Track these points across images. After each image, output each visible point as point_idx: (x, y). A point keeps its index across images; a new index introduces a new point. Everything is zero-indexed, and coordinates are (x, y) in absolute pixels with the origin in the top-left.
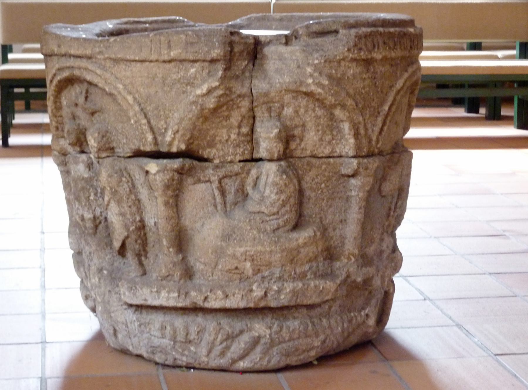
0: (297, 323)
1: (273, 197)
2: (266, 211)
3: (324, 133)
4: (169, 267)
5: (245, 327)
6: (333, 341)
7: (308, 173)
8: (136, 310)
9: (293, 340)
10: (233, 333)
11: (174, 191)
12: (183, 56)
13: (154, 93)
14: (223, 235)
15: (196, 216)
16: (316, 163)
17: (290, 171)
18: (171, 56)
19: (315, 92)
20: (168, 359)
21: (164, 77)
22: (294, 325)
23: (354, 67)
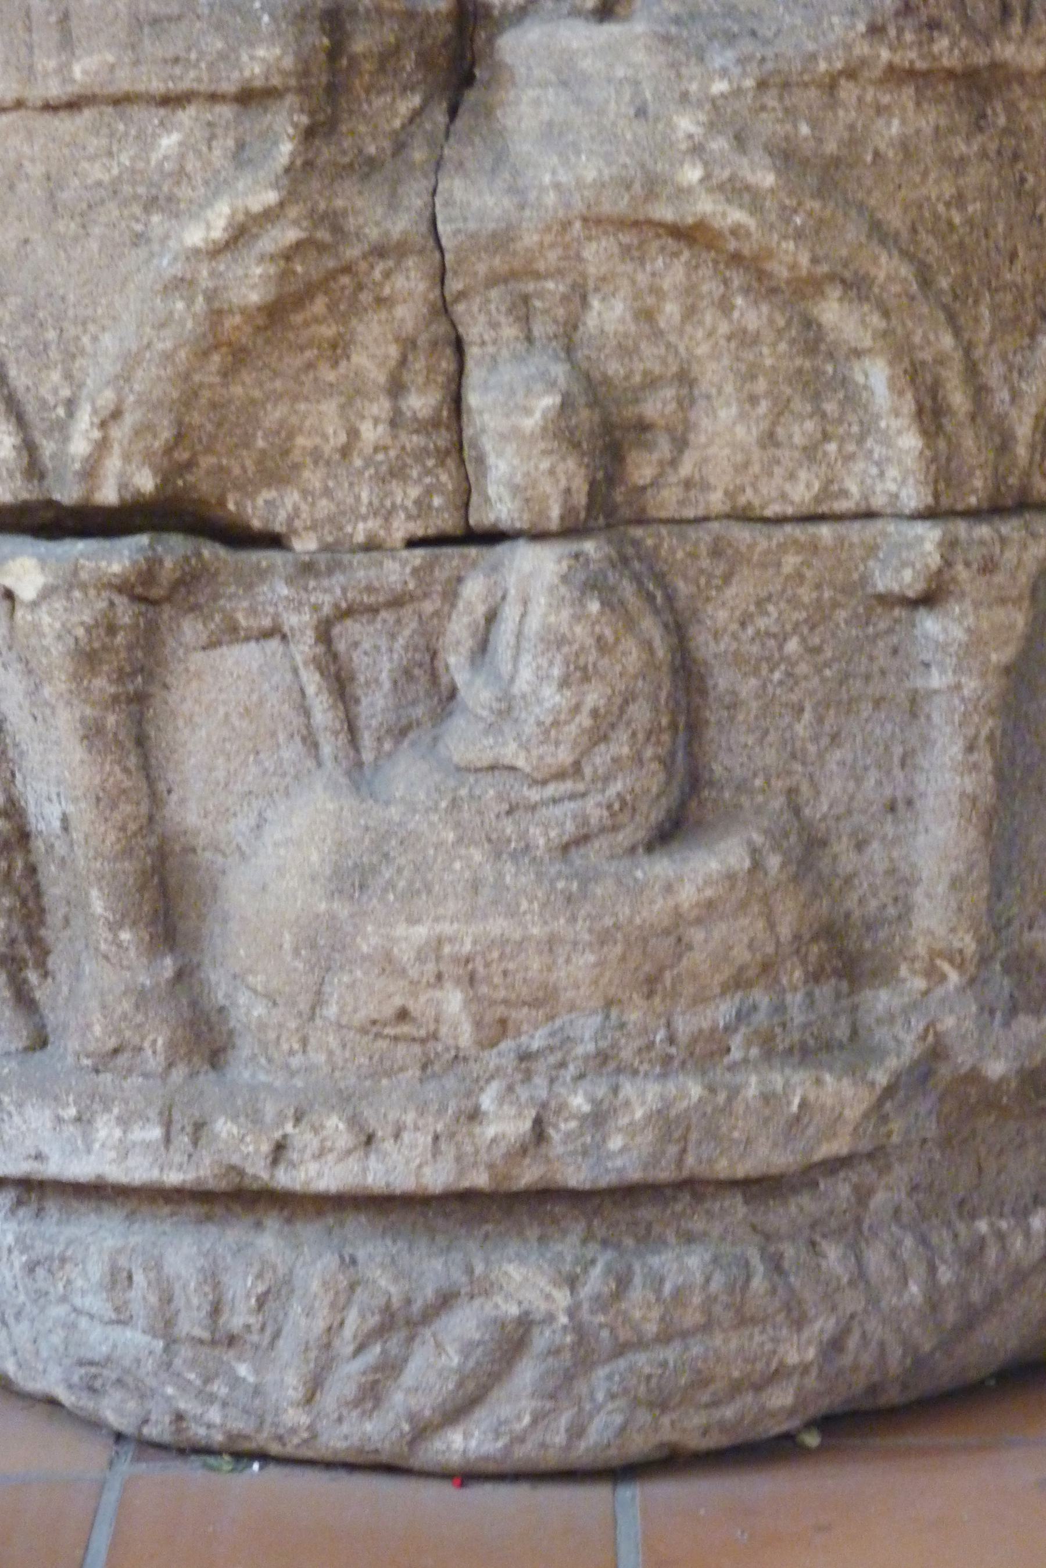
0: (695, 1261)
1: (552, 697)
2: (521, 763)
3: (781, 409)
4: (119, 1011)
5: (459, 1276)
6: (882, 1345)
7: (719, 589)
8: (19, 1203)
9: (685, 1335)
10: (408, 1302)
11: (121, 676)
12: (123, 82)
13: (13, 245)
14: (337, 873)
15: (226, 785)
16: (751, 547)
17: (625, 583)
18: (73, 81)
19: (717, 223)
20: (153, 1417)
21: (53, 172)
22: (680, 1271)
23: (904, 109)
